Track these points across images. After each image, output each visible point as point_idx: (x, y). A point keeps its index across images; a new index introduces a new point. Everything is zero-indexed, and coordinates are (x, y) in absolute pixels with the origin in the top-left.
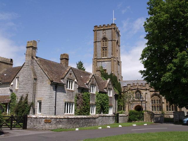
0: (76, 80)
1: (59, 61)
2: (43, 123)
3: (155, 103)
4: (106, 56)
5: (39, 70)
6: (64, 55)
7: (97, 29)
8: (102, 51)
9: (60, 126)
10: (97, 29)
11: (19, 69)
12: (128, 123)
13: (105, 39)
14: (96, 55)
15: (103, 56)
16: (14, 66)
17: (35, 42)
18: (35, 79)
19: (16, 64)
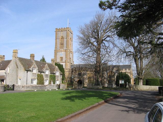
0: (37, 68)
1: (29, 58)
2: (21, 88)
3: (90, 78)
4: (63, 48)
5: (19, 64)
6: (32, 54)
7: (57, 30)
8: (60, 45)
9: (9, 112)
10: (57, 30)
11: (9, 62)
12: (146, 86)
13: (63, 38)
14: (56, 48)
15: (61, 48)
16: (6, 60)
17: (17, 50)
18: (18, 68)
19: (6, 59)
